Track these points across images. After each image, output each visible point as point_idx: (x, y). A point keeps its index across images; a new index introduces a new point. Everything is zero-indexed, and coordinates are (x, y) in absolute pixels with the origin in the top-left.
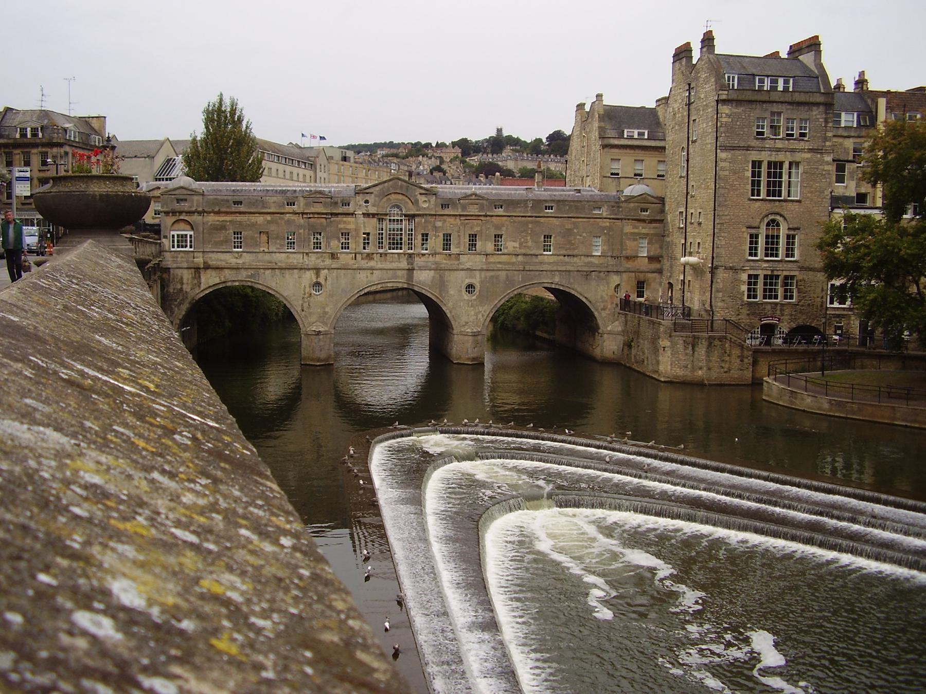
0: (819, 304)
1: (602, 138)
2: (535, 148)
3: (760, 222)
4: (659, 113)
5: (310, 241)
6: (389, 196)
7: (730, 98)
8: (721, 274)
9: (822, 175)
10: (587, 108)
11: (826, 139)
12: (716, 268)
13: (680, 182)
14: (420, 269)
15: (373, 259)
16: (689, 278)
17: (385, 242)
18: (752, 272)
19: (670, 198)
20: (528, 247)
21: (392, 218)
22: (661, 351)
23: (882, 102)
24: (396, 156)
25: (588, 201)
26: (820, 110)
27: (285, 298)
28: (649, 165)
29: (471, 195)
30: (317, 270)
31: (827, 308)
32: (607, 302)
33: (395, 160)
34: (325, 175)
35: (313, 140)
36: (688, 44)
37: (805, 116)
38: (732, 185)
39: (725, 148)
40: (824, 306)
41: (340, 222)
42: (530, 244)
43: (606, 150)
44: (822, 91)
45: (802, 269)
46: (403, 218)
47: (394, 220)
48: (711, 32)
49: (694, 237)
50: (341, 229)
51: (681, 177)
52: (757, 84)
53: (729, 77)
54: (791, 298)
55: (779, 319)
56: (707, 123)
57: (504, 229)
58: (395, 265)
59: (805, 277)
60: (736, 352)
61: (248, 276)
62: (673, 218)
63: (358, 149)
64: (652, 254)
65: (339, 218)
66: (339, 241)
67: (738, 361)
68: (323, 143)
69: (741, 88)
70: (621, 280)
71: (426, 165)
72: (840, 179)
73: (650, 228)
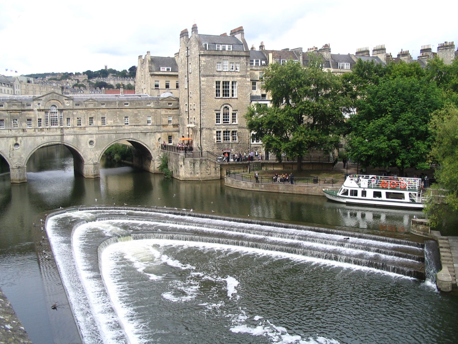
0: (248, 143)
1: (150, 71)
3: (221, 108)
6: (50, 101)
8: (204, 131)
9: (246, 87)
10: (143, 58)
11: (247, 71)
12: (202, 129)
15: (44, 131)
16: (191, 134)
18: (218, 130)
19: (181, 98)
20: (117, 123)
21: (52, 111)
22: (180, 167)
23: (271, 55)
24: (55, 79)
29: (90, 99)
32: (155, 146)
33: (55, 81)
36: (186, 30)
37: (238, 61)
38: (207, 92)
39: (204, 76)
40: (250, 144)
42: (118, 121)
43: (153, 76)
44: (245, 50)
45: (239, 128)
46: (57, 111)
48: (195, 25)
49: (192, 115)
51: (185, 89)
52: (217, 48)
53: (204, 45)
54: (236, 139)
56: (196, 65)
57: (106, 114)
59: (241, 131)
60: (213, 165)
62: (183, 108)
63: (36, 76)
64: (174, 123)
66: (26, 123)
67: (214, 169)
69: (210, 49)
71: (70, 83)
72: (254, 88)
73: (173, 112)
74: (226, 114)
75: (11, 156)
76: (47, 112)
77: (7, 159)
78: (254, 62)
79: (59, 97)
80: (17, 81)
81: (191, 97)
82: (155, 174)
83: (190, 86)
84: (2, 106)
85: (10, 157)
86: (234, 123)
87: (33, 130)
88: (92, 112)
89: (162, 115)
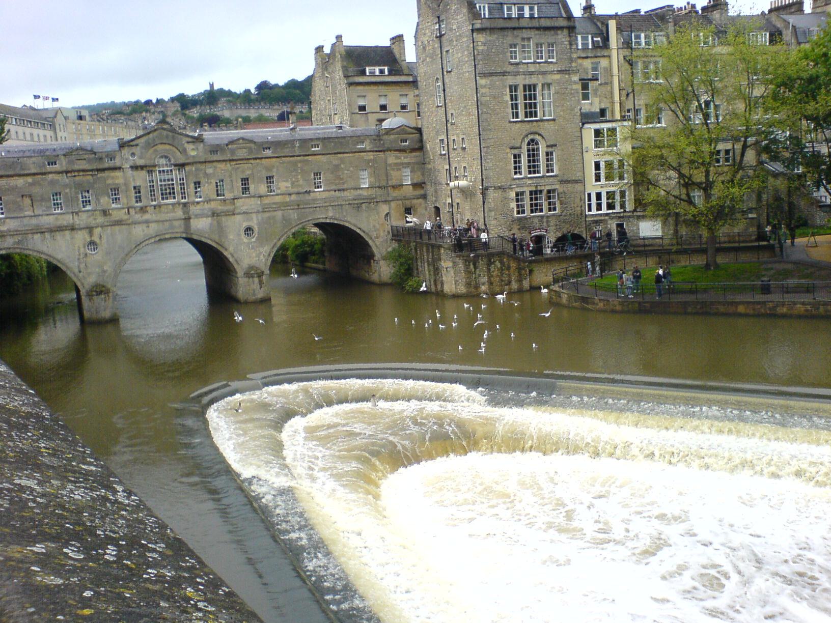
1: (346, 76)
2: (246, 98)
4: (394, 51)
5: (78, 200)
7: (484, 26)
8: (492, 194)
9: (571, 94)
10: (327, 50)
11: (571, 60)
12: (487, 189)
13: (437, 111)
14: (197, 216)
17: (158, 193)
18: (518, 190)
19: (428, 127)
20: (299, 186)
21: (161, 169)
22: (444, 272)
23: (612, 24)
25: (351, 137)
26: (564, 33)
27: (59, 261)
28: (394, 98)
29: (238, 139)
30: (90, 229)
31: (586, 215)
32: (379, 230)
34: (65, 134)
35: (46, 102)
39: (484, 75)
41: (108, 177)
42: (301, 182)
46: (173, 167)
47: (164, 171)
50: (109, 185)
51: (438, 106)
52: (506, 12)
53: (480, 7)
54: (555, 209)
55: (547, 230)
56: (464, 52)
57: (275, 170)
58: (171, 215)
59: (565, 189)
61: (15, 243)
64: (415, 181)
65: (107, 174)
66: (109, 197)
68: (56, 105)
70: (390, 208)
74: (534, 155)
75: (82, 270)
76: (152, 171)
77: (75, 275)
78: (643, 40)
79: (173, 137)
80: (59, 116)
81: (452, 124)
82: (382, 285)
83: (450, 99)
84: (56, 164)
85: (80, 272)
86: (518, 176)
87: (123, 211)
88: (246, 166)
89: (390, 165)
